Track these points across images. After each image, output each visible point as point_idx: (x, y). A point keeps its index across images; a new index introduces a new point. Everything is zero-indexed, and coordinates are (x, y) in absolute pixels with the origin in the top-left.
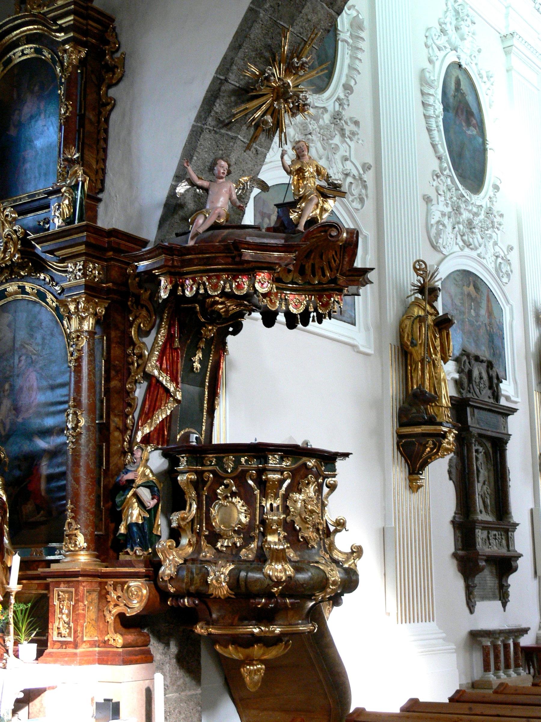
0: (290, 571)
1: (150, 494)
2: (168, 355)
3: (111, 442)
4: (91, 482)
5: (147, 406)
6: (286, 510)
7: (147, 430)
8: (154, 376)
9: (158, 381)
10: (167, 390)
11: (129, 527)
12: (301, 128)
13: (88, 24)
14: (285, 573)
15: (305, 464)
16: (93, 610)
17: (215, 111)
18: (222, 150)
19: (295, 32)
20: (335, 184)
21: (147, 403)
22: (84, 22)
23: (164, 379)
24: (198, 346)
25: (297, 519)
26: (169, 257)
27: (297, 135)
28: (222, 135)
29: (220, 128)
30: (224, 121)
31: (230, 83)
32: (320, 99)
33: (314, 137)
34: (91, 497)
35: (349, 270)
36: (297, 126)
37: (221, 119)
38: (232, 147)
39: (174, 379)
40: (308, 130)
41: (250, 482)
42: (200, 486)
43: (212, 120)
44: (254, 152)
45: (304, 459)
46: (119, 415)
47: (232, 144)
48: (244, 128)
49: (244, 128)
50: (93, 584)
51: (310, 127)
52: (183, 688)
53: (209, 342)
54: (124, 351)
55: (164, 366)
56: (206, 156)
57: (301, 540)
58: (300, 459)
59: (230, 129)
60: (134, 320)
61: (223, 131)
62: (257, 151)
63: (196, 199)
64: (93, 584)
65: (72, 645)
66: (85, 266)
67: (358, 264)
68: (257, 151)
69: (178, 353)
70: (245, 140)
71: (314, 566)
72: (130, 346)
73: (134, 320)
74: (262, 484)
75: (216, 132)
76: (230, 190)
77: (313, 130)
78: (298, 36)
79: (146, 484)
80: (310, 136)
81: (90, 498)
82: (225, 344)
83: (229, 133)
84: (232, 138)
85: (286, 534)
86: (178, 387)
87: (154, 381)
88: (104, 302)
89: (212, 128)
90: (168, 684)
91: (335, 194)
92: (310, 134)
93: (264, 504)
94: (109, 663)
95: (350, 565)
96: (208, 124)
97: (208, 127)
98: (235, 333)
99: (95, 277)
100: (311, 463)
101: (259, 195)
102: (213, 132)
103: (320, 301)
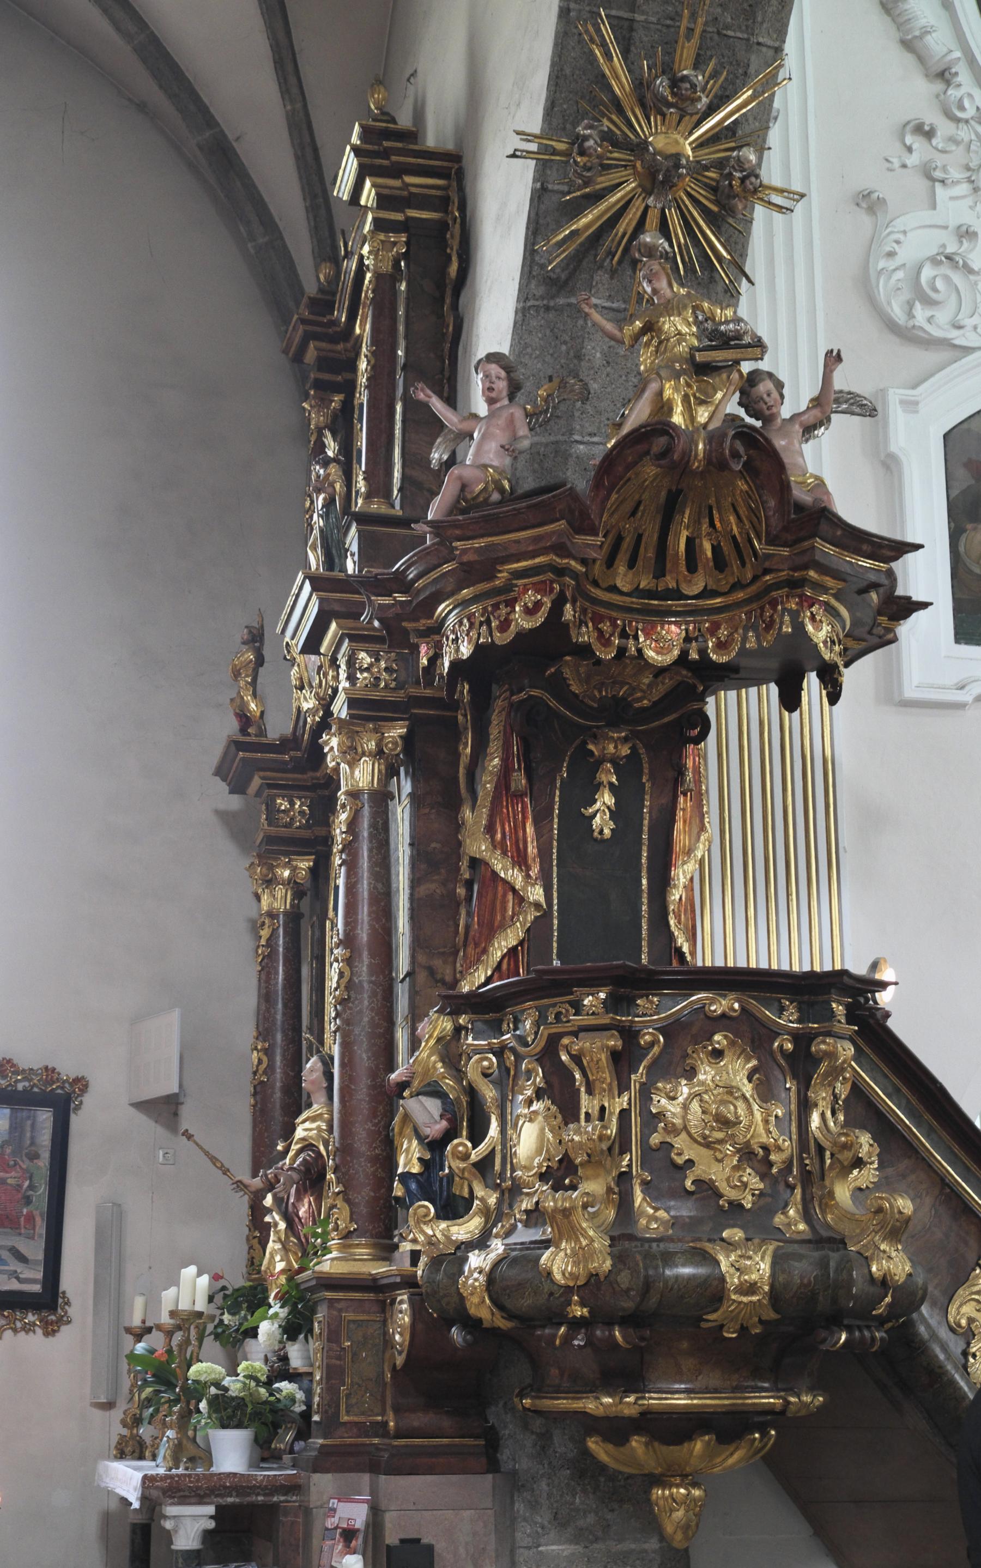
13: (407, 185)
18: (565, 343)
19: (654, 19)
20: (723, 334)
22: (397, 183)
24: (595, 782)
25: (679, 1142)
28: (559, 310)
29: (553, 297)
30: (558, 278)
31: (553, 191)
35: (785, 529)
46: (443, 953)
52: (600, 1534)
56: (539, 366)
61: (561, 301)
63: (536, 466)
69: (523, 803)
70: (615, 305)
75: (547, 308)
78: (668, 26)
79: (428, 1089)
90: (546, 1523)
101: (965, 426)
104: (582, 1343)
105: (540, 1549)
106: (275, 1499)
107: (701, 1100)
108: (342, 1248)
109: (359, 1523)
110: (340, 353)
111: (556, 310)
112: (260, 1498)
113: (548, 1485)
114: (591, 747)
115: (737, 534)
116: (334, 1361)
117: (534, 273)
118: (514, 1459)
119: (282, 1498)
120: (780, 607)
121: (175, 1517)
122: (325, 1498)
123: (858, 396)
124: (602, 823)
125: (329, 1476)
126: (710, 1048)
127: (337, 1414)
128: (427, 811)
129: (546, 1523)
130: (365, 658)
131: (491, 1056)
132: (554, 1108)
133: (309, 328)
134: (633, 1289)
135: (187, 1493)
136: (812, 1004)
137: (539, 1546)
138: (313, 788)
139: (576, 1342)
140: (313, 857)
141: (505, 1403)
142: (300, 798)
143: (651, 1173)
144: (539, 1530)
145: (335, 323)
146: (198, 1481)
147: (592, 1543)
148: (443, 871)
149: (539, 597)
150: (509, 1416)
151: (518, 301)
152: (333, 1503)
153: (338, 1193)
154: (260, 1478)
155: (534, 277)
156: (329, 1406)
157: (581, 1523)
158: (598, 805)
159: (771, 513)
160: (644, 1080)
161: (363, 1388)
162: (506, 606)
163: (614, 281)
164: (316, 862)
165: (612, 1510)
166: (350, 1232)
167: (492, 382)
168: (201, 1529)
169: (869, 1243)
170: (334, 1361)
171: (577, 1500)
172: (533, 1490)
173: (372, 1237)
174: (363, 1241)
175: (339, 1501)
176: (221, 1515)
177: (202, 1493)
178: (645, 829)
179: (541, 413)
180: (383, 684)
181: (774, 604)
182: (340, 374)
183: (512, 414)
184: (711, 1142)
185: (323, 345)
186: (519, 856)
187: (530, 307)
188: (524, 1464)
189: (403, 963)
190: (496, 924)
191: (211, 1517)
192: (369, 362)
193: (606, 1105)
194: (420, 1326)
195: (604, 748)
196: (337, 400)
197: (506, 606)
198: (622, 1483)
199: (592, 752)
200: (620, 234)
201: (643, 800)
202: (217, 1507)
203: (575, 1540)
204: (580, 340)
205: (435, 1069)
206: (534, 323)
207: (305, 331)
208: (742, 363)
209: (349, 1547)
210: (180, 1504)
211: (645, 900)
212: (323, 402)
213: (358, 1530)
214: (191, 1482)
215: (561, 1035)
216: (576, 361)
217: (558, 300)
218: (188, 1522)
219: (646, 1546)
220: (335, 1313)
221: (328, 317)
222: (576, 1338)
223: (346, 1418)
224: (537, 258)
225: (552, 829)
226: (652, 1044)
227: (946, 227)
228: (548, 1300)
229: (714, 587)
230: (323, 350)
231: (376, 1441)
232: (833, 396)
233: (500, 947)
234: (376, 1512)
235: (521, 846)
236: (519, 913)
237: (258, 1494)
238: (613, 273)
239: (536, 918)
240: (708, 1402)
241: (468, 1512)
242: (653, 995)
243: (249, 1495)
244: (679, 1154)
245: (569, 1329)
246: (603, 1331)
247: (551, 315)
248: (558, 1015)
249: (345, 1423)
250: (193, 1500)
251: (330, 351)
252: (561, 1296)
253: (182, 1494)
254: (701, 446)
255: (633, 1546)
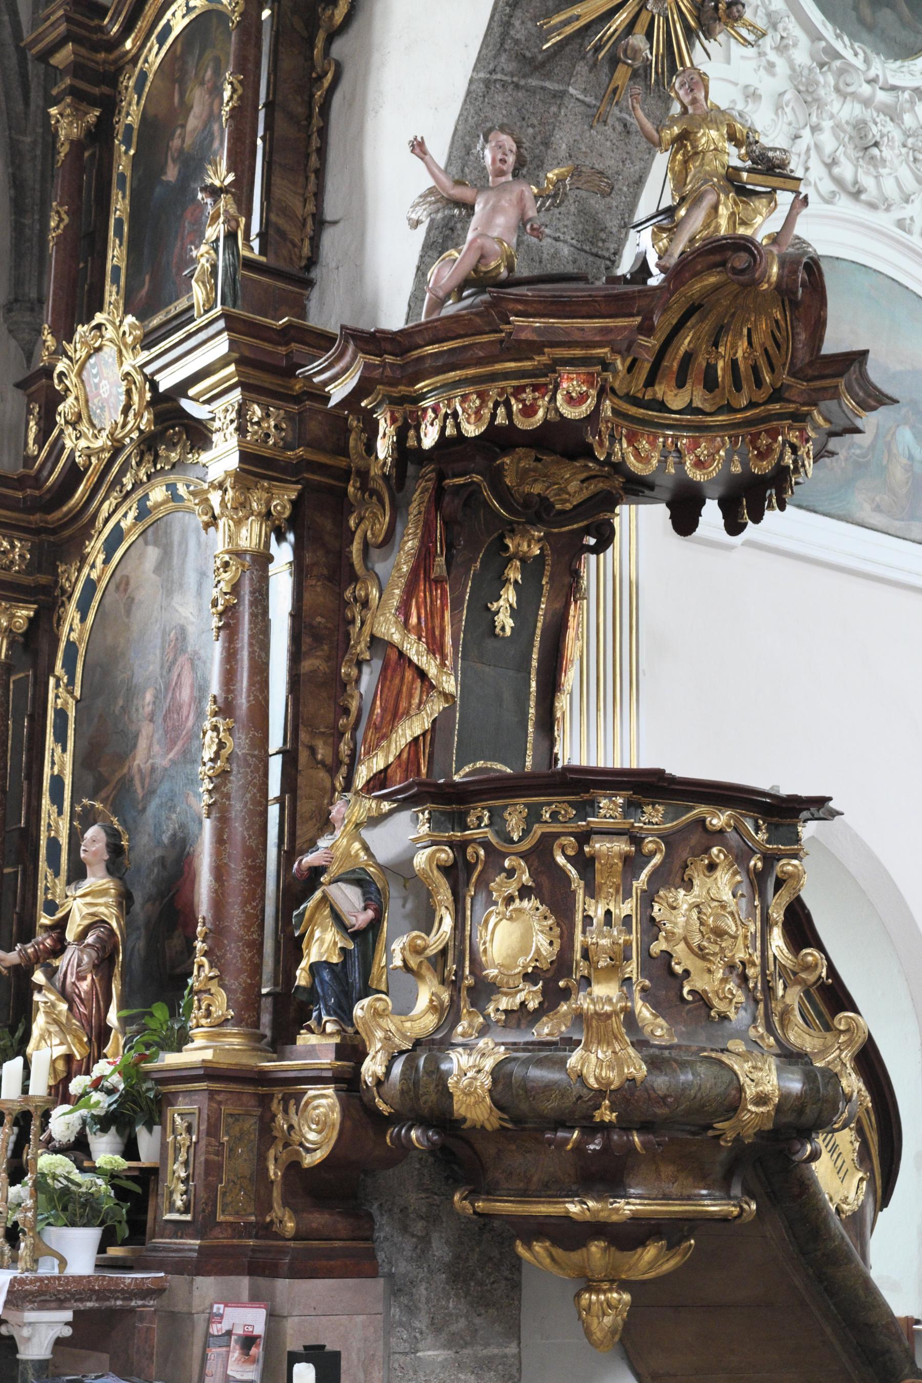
0: (638, 1069)
1: (361, 899)
2: (422, 594)
3: (299, 792)
4: (248, 875)
5: (378, 711)
6: (652, 927)
7: (378, 763)
8: (391, 645)
9: (401, 654)
10: (422, 674)
11: (314, 968)
12: (854, 133)
14: (621, 1071)
15: (701, 822)
16: (245, 1156)
17: (512, 38)
18: (533, 126)
20: (770, 160)
21: (378, 703)
23: (415, 651)
25: (680, 950)
26: (376, 360)
27: (841, 149)
28: (531, 91)
29: (525, 76)
32: (904, 69)
33: (887, 153)
34: (248, 908)
35: (811, 364)
36: (844, 131)
37: (528, 54)
38: (556, 115)
39: (435, 647)
40: (870, 136)
41: (561, 860)
42: (462, 876)
43: (509, 60)
44: (619, 128)
45: (700, 810)
47: (554, 109)
48: (582, 68)
49: (582, 68)
50: (245, 1099)
51: (874, 129)
52: (468, 1339)
53: (533, 568)
54: (341, 595)
55: (414, 620)
57: (690, 998)
58: (692, 808)
59: (548, 76)
60: (358, 525)
61: (534, 82)
62: (625, 126)
64: (245, 1099)
65: (190, 1231)
66: (243, 412)
67: (831, 345)
68: (625, 126)
69: (443, 591)
70: (587, 99)
71: (711, 1058)
72: (350, 584)
73: (358, 525)
74: (585, 864)
75: (517, 86)
76: (521, 199)
77: (882, 137)
80: (875, 151)
81: (244, 912)
82: (576, 575)
83: (547, 84)
84: (554, 96)
85: (647, 983)
86: (445, 665)
87: (394, 656)
88: (286, 489)
89: (508, 79)
90: (424, 1328)
91: (775, 185)
92: (876, 144)
93: (591, 913)
94: (267, 1272)
95: (829, 1063)
96: (498, 69)
97: (499, 76)
98: (598, 549)
99: (268, 435)
100: (719, 819)
102: (511, 86)
103: (755, 448)
104: (598, 1148)
105: (419, 1354)
106: (133, 1304)
107: (699, 913)
108: (210, 1036)
109: (259, 1329)
110: (97, 63)
111: (527, 91)
112: (119, 1303)
113: (426, 1289)
114: (508, 542)
115: (740, 360)
116: (212, 1157)
117: (507, 47)
118: (390, 1263)
119: (140, 1303)
120: (780, 438)
121: (30, 1323)
122: (207, 1303)
123: (804, 242)
124: (505, 621)
125: (211, 1279)
126: (706, 862)
127: (214, 1213)
128: (314, 582)
129: (424, 1328)
130: (257, 411)
131: (447, 848)
132: (542, 908)
133: (75, 29)
134: (670, 1096)
135: (48, 1298)
136: (777, 826)
137: (417, 1351)
138: (37, 531)
139: (592, 1147)
140: (35, 606)
141: (381, 1205)
142: (20, 540)
143: (650, 980)
144: (418, 1335)
145: (101, 30)
146: (67, 1284)
147: (462, 1348)
148: (326, 647)
149: (585, 389)
150: (385, 1217)
151: (475, 69)
152: (218, 1308)
153: (212, 978)
154: (128, 1281)
155: (505, 50)
156: (207, 1204)
157: (454, 1328)
158: (501, 602)
159: (800, 346)
160: (645, 887)
161: (238, 1187)
162: (533, 391)
163: (592, 75)
164: (37, 612)
165: (479, 1315)
166: (227, 1020)
167: (505, 154)
168: (55, 1337)
169: (835, 1059)
170: (212, 1157)
171: (451, 1305)
172: (412, 1295)
173: (247, 1025)
174: (235, 1030)
175: (226, 1306)
176: (80, 1320)
177: (62, 1297)
178: (538, 632)
179: (548, 197)
180: (271, 442)
181: (773, 434)
182: (98, 86)
183: (522, 191)
184: (708, 954)
185: (83, 51)
186: (434, 643)
187: (496, 81)
188: (402, 1267)
189: (276, 740)
190: (401, 711)
191: (67, 1324)
192: (234, 91)
193: (612, 909)
194: (348, 1124)
195: (519, 545)
196: (93, 115)
197: (533, 391)
198: (489, 1287)
199: (507, 547)
200: (612, 30)
201: (539, 602)
202: (75, 1312)
203: (448, 1345)
204: (551, 127)
205: (357, 855)
206: (499, 98)
207: (68, 30)
208: (778, 192)
209: (248, 1354)
210: (40, 1309)
211: (532, 704)
212: (79, 114)
213: (258, 1337)
214: (60, 1285)
215: (557, 835)
216: (542, 148)
217: (530, 81)
218: (43, 1328)
219: (507, 1351)
220: (215, 1105)
221: (96, 22)
222: (592, 1143)
223: (220, 1218)
224: (512, 32)
225: (461, 620)
226: (652, 854)
227: (736, 84)
228: (575, 1103)
229: (700, 406)
230: (83, 57)
231: (251, 1242)
232: (791, 240)
233: (404, 735)
234: (273, 1317)
235: (437, 633)
236: (427, 702)
237: (117, 1299)
238: (594, 66)
239: (444, 709)
240: (659, 1208)
241: (361, 1318)
242: (659, 804)
243: (108, 1299)
244: (678, 964)
245: (582, 1133)
246: (620, 1137)
247: (520, 94)
248: (554, 815)
249: (220, 1223)
250: (53, 1305)
251: (88, 59)
252: (590, 1100)
253: (43, 1298)
254: (775, 269)
255: (496, 1351)
